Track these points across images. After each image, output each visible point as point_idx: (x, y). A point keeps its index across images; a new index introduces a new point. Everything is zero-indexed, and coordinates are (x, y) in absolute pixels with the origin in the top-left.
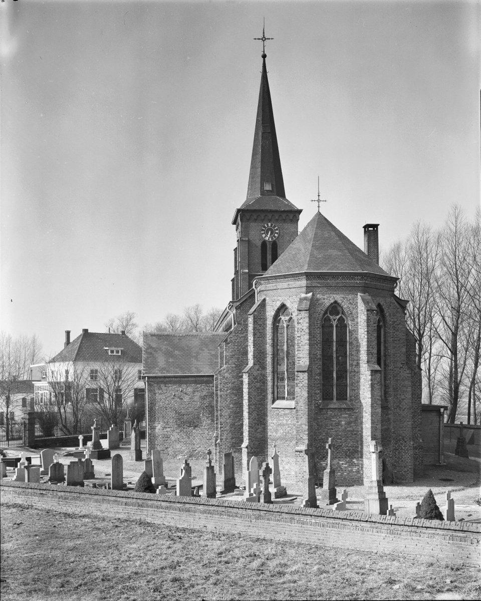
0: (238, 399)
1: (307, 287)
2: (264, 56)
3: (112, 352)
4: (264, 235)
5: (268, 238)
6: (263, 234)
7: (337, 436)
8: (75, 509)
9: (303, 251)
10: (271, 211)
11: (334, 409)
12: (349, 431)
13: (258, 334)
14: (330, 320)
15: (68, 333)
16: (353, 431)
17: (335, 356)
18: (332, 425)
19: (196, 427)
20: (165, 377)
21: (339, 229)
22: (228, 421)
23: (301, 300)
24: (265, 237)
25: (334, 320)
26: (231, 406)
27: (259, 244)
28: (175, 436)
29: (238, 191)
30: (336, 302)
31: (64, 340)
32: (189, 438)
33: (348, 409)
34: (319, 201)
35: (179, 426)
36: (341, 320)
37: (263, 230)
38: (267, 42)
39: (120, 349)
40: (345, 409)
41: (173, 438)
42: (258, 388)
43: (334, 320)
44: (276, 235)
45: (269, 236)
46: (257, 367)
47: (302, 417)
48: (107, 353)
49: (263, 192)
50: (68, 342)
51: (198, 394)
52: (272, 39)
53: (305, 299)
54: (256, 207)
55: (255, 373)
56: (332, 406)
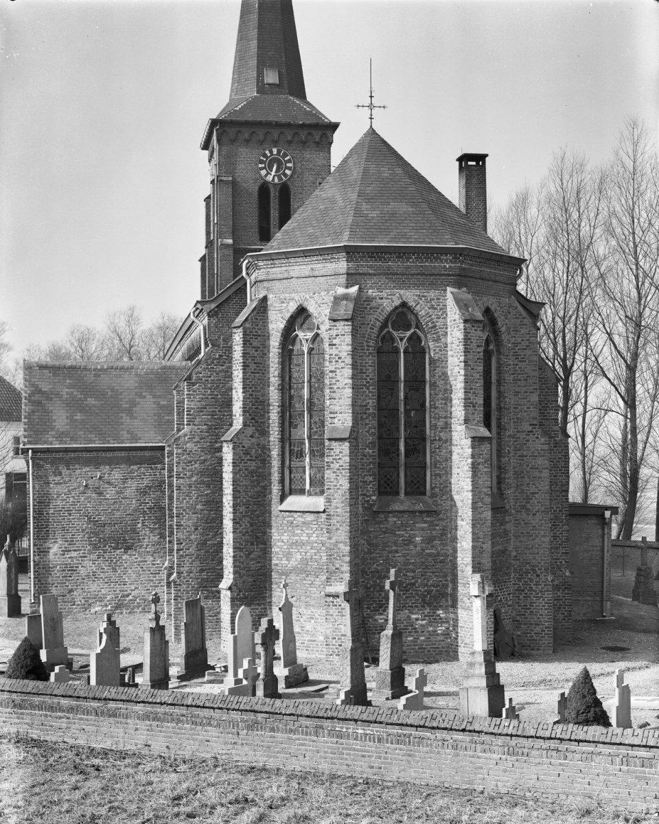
4: (263, 172)
6: (262, 169)
9: (341, 203)
10: (278, 125)
12: (430, 555)
13: (253, 366)
14: (392, 339)
16: (438, 554)
18: (395, 544)
19: (128, 548)
20: (66, 450)
23: (337, 300)
24: (266, 175)
26: (199, 507)
28: (87, 567)
30: (404, 304)
32: (115, 570)
33: (427, 512)
34: (371, 106)
35: (96, 547)
36: (415, 339)
37: (261, 162)
40: (421, 512)
41: (83, 571)
42: (251, 472)
43: (401, 339)
44: (288, 172)
45: (273, 173)
47: (337, 529)
49: (262, 88)
53: (345, 297)
54: (249, 117)
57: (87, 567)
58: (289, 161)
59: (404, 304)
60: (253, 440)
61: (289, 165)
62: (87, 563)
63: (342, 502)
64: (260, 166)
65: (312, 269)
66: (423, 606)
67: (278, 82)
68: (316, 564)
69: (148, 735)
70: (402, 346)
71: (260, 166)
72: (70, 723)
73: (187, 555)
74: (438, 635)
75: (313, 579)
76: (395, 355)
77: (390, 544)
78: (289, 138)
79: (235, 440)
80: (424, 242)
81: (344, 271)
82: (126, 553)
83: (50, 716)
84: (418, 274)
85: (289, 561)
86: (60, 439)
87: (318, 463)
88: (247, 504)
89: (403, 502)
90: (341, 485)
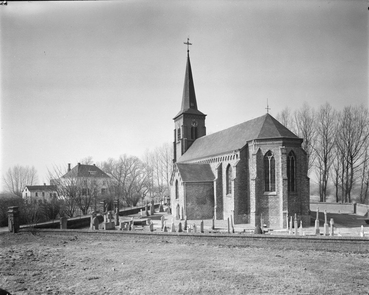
2: (188, 51)
3: (92, 173)
4: (192, 124)
5: (194, 126)
10: (193, 114)
15: (69, 165)
20: (192, 182)
21: (205, 123)
23: (281, 149)
27: (191, 127)
29: (177, 106)
31: (67, 168)
34: (268, 109)
35: (198, 204)
36: (273, 157)
37: (192, 122)
39: (95, 172)
41: (195, 209)
44: (197, 125)
48: (90, 173)
49: (190, 106)
50: (69, 169)
54: (189, 112)
59: (292, 151)
80: (267, 137)
89: (292, 193)
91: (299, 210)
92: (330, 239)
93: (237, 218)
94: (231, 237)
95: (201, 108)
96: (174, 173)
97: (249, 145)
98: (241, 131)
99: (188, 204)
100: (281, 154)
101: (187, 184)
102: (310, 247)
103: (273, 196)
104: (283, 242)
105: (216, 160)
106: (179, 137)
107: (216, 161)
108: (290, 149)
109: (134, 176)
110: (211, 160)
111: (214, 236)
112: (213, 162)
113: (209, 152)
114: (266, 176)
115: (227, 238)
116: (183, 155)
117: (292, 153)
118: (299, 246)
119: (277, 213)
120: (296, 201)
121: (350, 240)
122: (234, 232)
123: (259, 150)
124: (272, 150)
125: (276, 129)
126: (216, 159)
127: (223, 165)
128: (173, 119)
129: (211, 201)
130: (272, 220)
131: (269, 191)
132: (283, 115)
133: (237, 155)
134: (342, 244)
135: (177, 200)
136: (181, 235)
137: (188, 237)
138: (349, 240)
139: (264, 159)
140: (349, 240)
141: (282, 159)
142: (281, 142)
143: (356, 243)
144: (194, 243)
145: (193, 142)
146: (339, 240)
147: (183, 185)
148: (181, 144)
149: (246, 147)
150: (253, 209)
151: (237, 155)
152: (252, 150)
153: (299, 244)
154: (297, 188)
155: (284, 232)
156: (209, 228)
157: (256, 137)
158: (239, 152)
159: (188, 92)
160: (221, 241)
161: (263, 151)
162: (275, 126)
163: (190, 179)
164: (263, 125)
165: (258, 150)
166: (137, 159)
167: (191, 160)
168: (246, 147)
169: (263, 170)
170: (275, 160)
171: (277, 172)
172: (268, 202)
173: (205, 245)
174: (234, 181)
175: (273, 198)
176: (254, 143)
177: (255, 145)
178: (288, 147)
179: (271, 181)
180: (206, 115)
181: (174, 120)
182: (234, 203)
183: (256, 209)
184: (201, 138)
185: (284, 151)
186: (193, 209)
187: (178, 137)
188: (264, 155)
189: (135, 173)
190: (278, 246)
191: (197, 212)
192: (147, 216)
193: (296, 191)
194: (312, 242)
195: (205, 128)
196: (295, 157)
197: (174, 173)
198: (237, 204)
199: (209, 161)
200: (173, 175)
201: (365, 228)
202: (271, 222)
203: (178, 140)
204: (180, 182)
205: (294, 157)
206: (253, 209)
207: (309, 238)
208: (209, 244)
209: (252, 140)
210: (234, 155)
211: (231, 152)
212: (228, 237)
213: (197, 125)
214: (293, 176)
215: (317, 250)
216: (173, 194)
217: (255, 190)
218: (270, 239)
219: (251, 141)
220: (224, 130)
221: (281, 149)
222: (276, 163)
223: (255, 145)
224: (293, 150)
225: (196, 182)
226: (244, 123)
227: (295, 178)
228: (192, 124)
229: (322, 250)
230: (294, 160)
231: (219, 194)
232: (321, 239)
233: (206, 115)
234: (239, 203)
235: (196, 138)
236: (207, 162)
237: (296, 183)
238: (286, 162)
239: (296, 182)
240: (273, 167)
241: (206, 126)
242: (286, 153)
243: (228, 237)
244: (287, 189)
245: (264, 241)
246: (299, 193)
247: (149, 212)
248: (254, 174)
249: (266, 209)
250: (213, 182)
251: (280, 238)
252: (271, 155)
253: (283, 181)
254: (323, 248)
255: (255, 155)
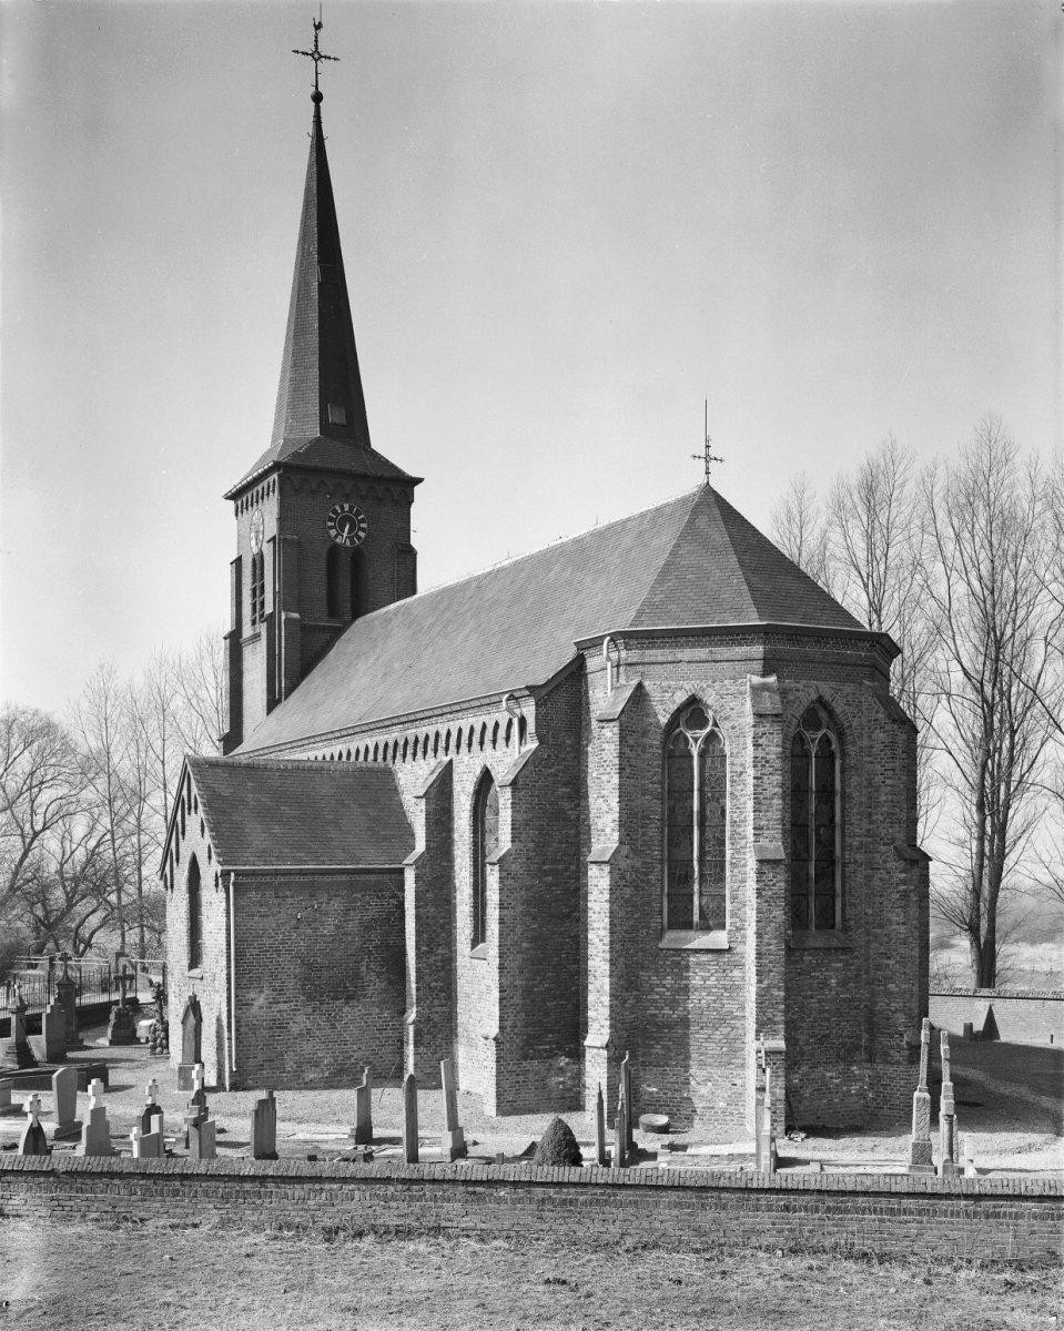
0: (540, 927)
1: (764, 659)
2: (317, 98)
6: (331, 528)
7: (821, 1011)
8: (602, 1230)
11: (816, 949)
12: (844, 1000)
13: (628, 770)
16: (853, 1000)
17: (813, 825)
18: (811, 989)
19: (349, 998)
20: (277, 873)
22: (517, 983)
23: (757, 691)
24: (336, 536)
25: (695, 740)
26: (525, 945)
28: (299, 1023)
29: (252, 420)
32: (333, 1027)
33: (843, 949)
35: (310, 998)
37: (331, 519)
38: (323, 64)
40: (836, 949)
41: (295, 1029)
42: (626, 901)
43: (696, 740)
44: (362, 534)
45: (345, 535)
46: (625, 850)
47: (770, 971)
49: (325, 426)
51: (355, 916)
52: (335, 59)
54: (316, 462)
55: (623, 865)
56: (811, 943)
57: (299, 1023)
58: (363, 521)
59: (820, 700)
60: (629, 861)
61: (364, 525)
62: (301, 1018)
63: (775, 938)
64: (330, 524)
65: (711, 652)
66: (837, 1062)
67: (345, 422)
68: (715, 1013)
69: (1050, 1238)
70: (814, 750)
71: (330, 524)
72: (925, 1228)
73: (511, 1005)
74: (852, 1095)
75: (710, 1032)
76: (804, 759)
77: (806, 988)
78: (364, 493)
79: (613, 861)
81: (761, 657)
82: (347, 1003)
83: (889, 1220)
84: (834, 663)
85: (674, 1011)
86: (263, 859)
87: (711, 889)
88: (622, 941)
89: (816, 939)
90: (774, 917)
91: (859, 1037)
92: (865, 1193)
93: (513, 1078)
94: (344, 1180)
95: (392, 434)
96: (179, 818)
97: (592, 663)
98: (569, 582)
99: (252, 995)
100: (750, 720)
101: (241, 885)
102: (760, 1233)
103: (710, 957)
104: (620, 1205)
105: (418, 747)
106: (258, 606)
107: (425, 753)
108: (808, 691)
109: (27, 827)
110: (401, 743)
111: (253, 1178)
112: (409, 756)
113: (400, 700)
114: (673, 843)
115: (327, 1186)
116: (277, 711)
117: (823, 714)
118: (706, 1227)
119: (733, 1048)
120: (843, 983)
121: (967, 1197)
122: (459, 1151)
123: (639, 696)
124: (710, 698)
125: (738, 580)
126: (421, 739)
127: (456, 777)
128: (228, 498)
129: (390, 983)
130: (703, 1090)
131: (688, 925)
132: (870, 489)
133: (523, 721)
134: (925, 1219)
135: (196, 972)
136: (77, 1172)
137: (117, 1182)
138: (958, 1196)
139: (664, 744)
140: (958, 1196)
141: (756, 745)
142: (757, 650)
143: (997, 1215)
144: (143, 1214)
145: (337, 633)
146: (909, 1195)
147: (220, 886)
148: (262, 645)
149: (574, 676)
150: (598, 1033)
151: (523, 721)
152: (605, 696)
153: (706, 1218)
154: (850, 912)
155: (740, 1155)
156: (333, 1137)
157: (623, 623)
158: (532, 702)
159: (313, 340)
160: (290, 1203)
161: (662, 702)
162: (734, 559)
163: (263, 856)
164: (673, 554)
165: (628, 693)
166: (48, 729)
167: (312, 740)
168: (574, 676)
169: (657, 809)
170: (722, 750)
171: (734, 822)
172: (686, 990)
173: (202, 1229)
174: (497, 868)
175: (713, 968)
176: (614, 656)
177: (618, 666)
178: (797, 679)
179: (700, 870)
180: (420, 480)
181: (231, 503)
182: (496, 994)
183: (612, 1026)
184: (385, 609)
185: (770, 703)
186: (279, 1025)
187: (254, 605)
188: (664, 720)
189: (33, 812)
190: (598, 1227)
191: (307, 1047)
192: (17, 1067)
193: (846, 929)
194: (770, 1209)
195: (411, 554)
196: (841, 735)
197: (179, 818)
198: (517, 1000)
199: (390, 751)
200: (175, 829)
201: (89, 1113)
202: (699, 1105)
203: (254, 623)
204: (210, 870)
205: (832, 736)
206: (598, 1033)
207: (755, 1186)
208: (225, 1224)
209: (603, 637)
210: (510, 720)
211: (489, 702)
212: (332, 1180)
213: (362, 534)
214: (827, 846)
215: (794, 1251)
216: (175, 945)
217: (607, 920)
218: (551, 1191)
219: (595, 643)
220: (494, 575)
221: (757, 691)
222: (728, 769)
223: (618, 666)
224: (827, 698)
225: (301, 873)
226: (592, 534)
227: (838, 852)
228: (336, 530)
229: (815, 1251)
230: (832, 756)
231: (431, 939)
232: (820, 1192)
233: (420, 480)
234: (527, 992)
235: (358, 612)
236: (361, 758)
237: (843, 885)
238: (778, 764)
239: (843, 877)
240: (714, 791)
241: (415, 542)
242: (777, 715)
243: (332, 1180)
244: (779, 914)
245: (520, 1200)
246: (858, 937)
247: (38, 1044)
248: (608, 830)
249: (670, 1028)
250: (401, 872)
251: (606, 1185)
252: (702, 723)
253: (760, 873)
254: (828, 1242)
255: (611, 724)
